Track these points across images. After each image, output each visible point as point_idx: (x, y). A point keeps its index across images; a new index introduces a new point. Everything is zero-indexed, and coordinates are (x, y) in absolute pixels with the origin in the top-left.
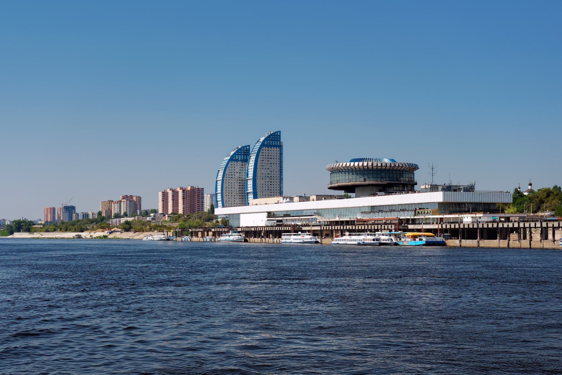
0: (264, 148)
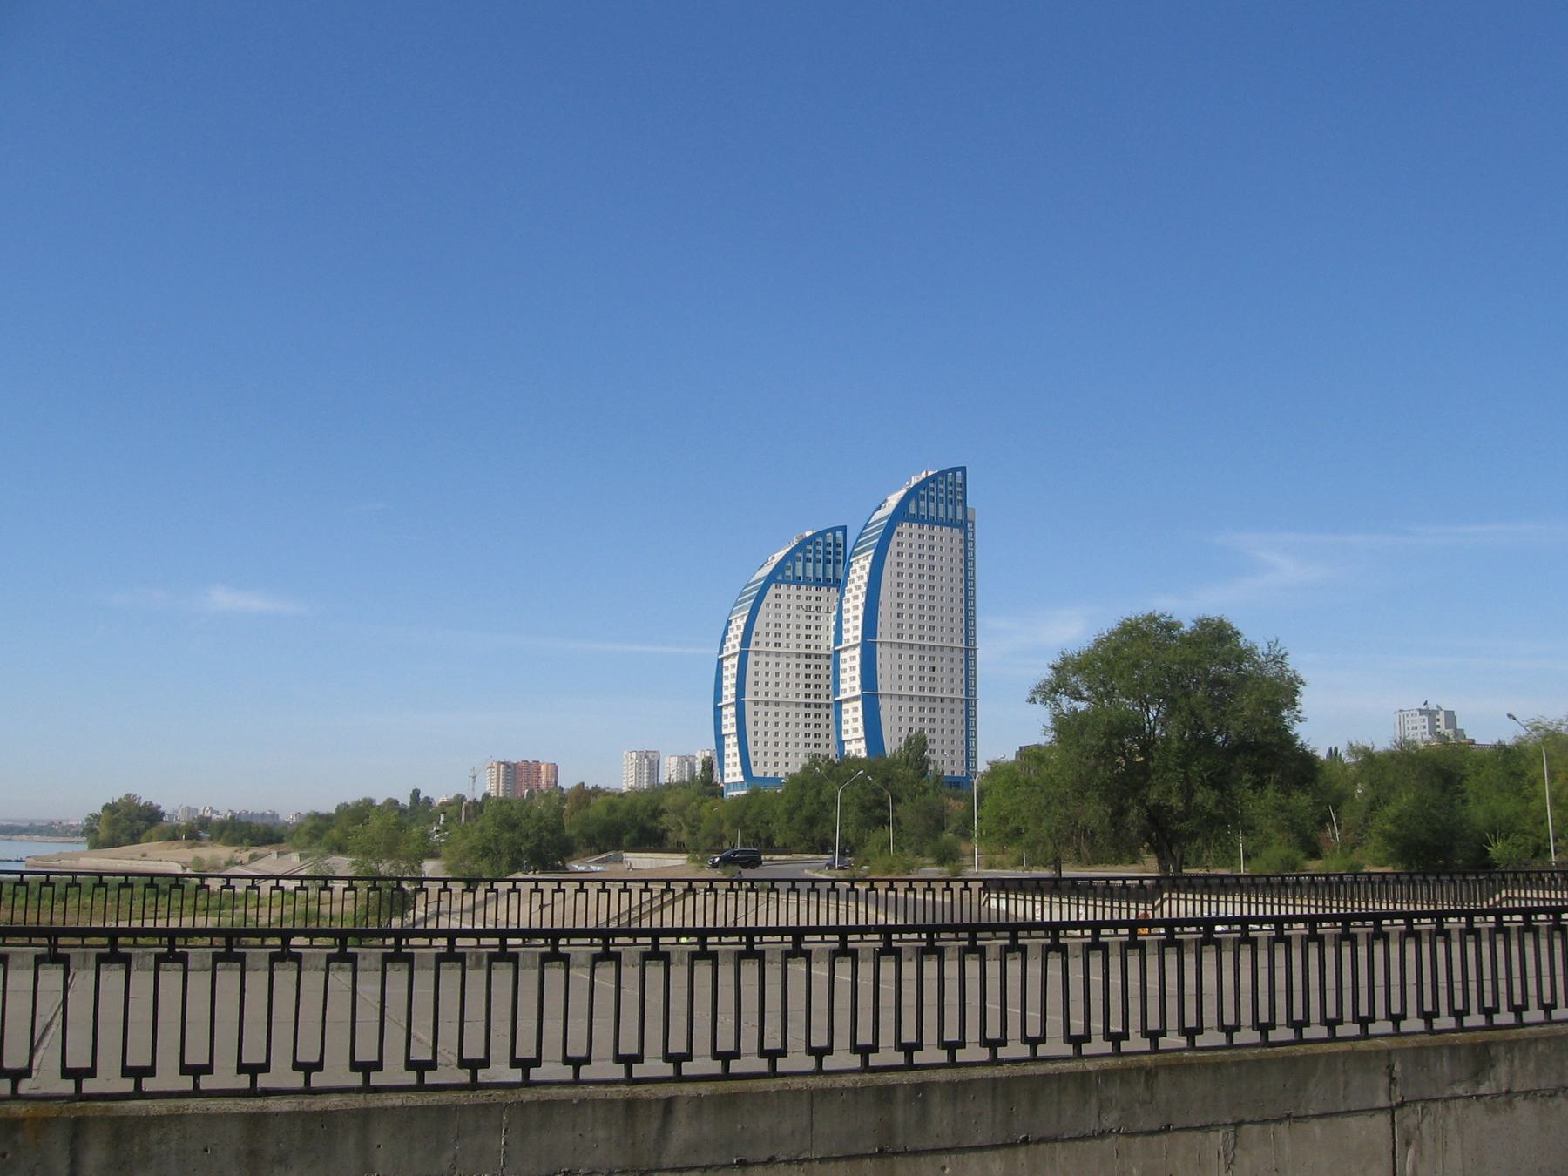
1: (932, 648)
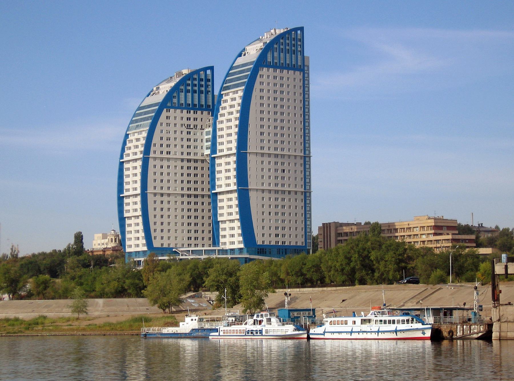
0: (264, 71)
1: (283, 156)
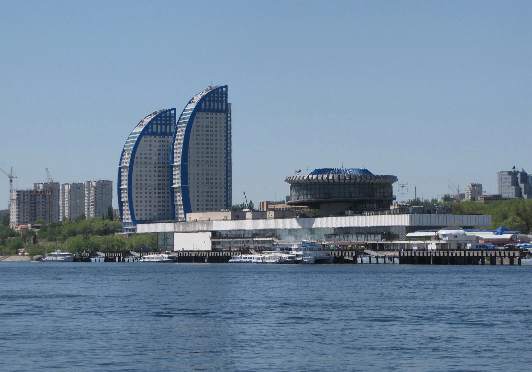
0: (199, 115)
